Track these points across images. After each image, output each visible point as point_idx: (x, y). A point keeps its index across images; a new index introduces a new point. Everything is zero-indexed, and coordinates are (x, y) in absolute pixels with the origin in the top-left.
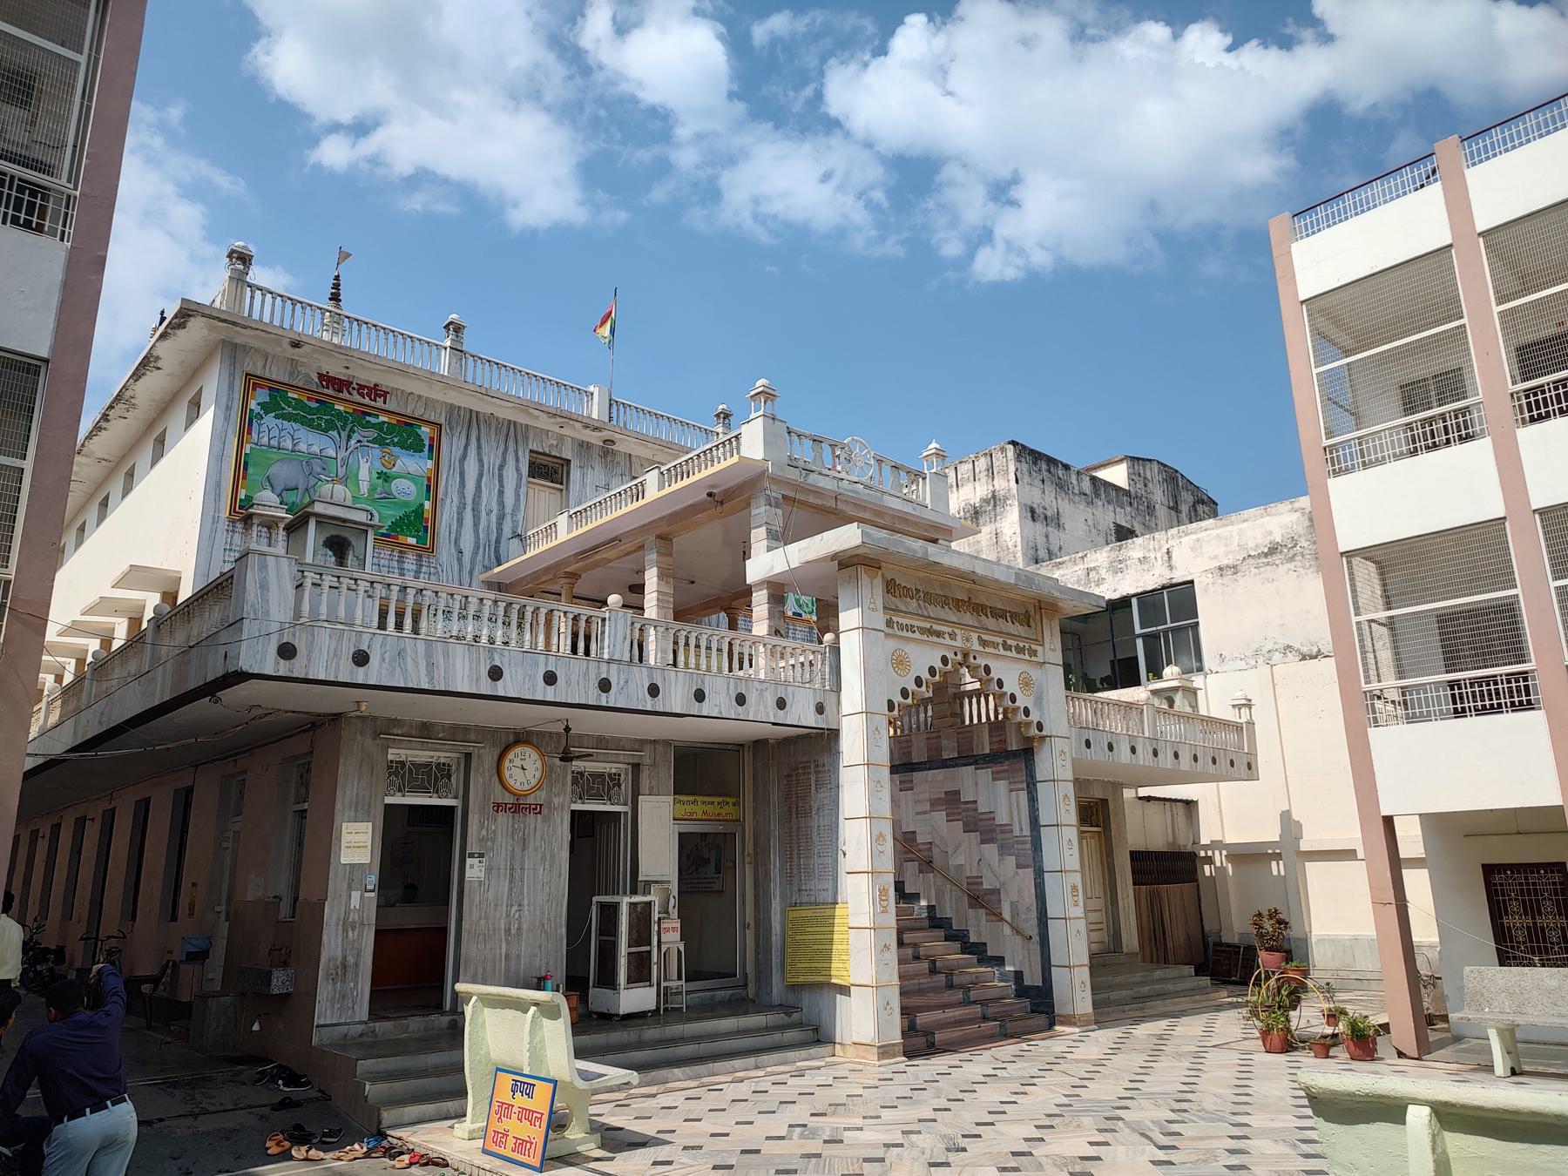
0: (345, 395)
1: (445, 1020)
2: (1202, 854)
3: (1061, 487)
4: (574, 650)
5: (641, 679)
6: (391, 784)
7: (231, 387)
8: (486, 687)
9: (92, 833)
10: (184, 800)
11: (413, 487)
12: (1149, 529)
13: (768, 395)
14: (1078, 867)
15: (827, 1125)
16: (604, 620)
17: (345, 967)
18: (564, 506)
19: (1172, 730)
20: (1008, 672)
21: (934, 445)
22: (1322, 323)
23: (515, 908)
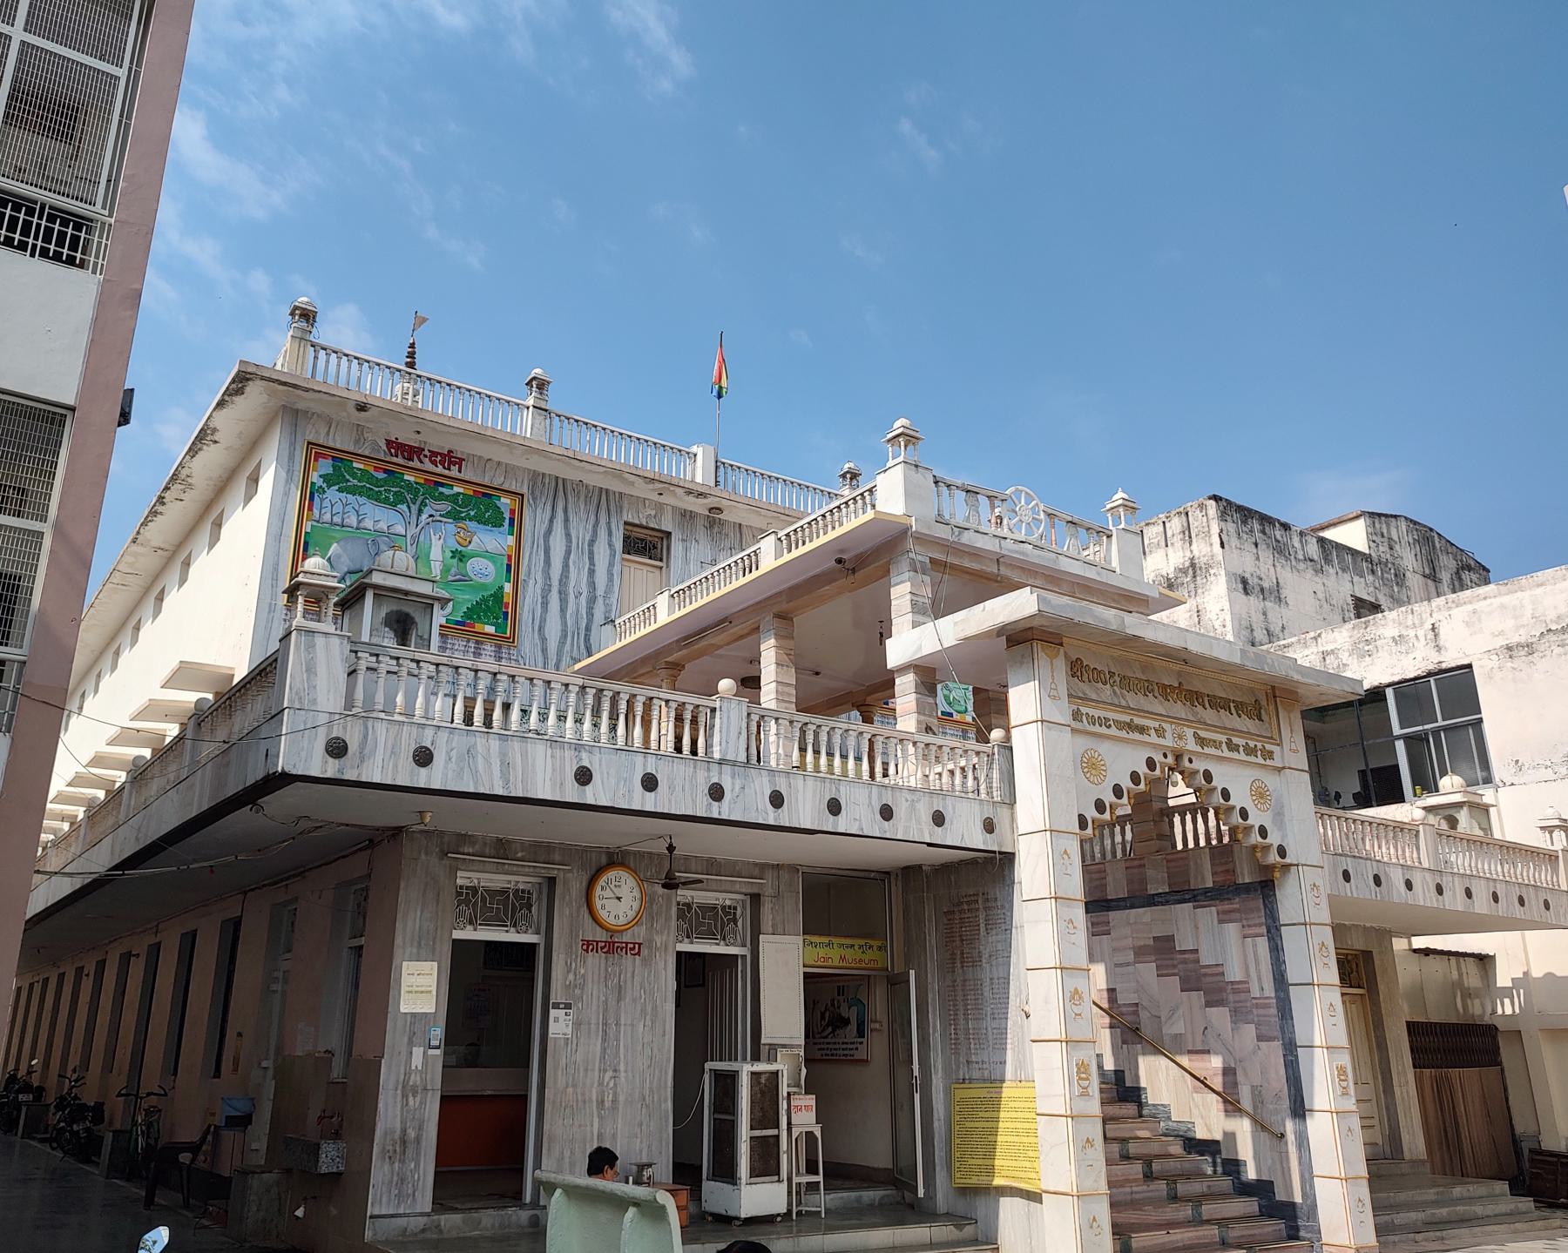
0: (416, 464)
1: (524, 1216)
3: (1280, 552)
5: (761, 787)
6: (460, 915)
7: (291, 457)
8: (572, 793)
9: (87, 985)
10: (233, 929)
12: (1398, 602)
13: (909, 438)
16: (713, 710)
17: (404, 1142)
21: (1121, 494)
23: (610, 1074)
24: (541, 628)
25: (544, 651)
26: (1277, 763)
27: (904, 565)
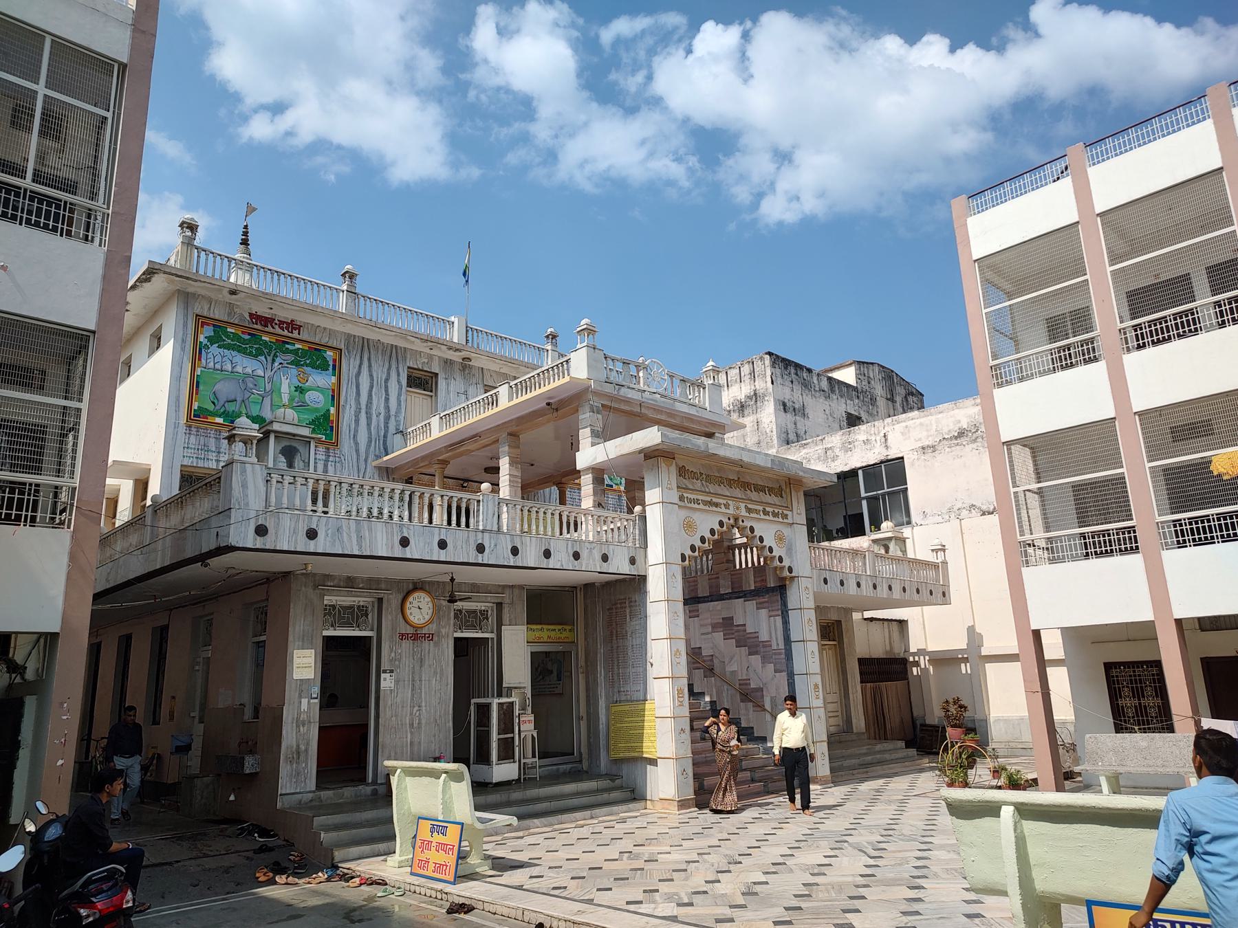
0: (270, 329)
1: (369, 789)
2: (911, 659)
3: (806, 386)
4: (449, 523)
7: (185, 325)
8: (398, 552)
11: (321, 397)
12: (873, 416)
13: (590, 331)
14: (818, 671)
15: (646, 851)
16: (478, 501)
17: (298, 753)
18: (434, 411)
19: (887, 569)
20: (767, 531)
21: (711, 363)
22: (989, 274)
24: (355, 436)
25: (357, 451)
26: (790, 521)
27: (587, 408)
